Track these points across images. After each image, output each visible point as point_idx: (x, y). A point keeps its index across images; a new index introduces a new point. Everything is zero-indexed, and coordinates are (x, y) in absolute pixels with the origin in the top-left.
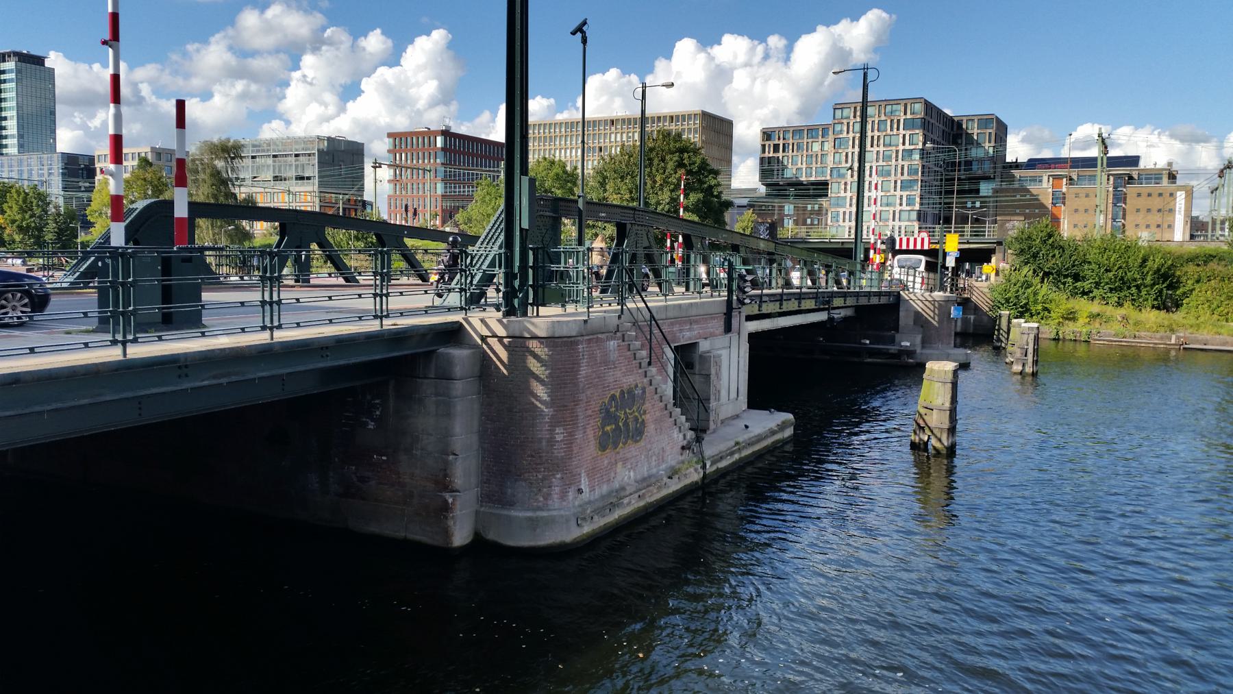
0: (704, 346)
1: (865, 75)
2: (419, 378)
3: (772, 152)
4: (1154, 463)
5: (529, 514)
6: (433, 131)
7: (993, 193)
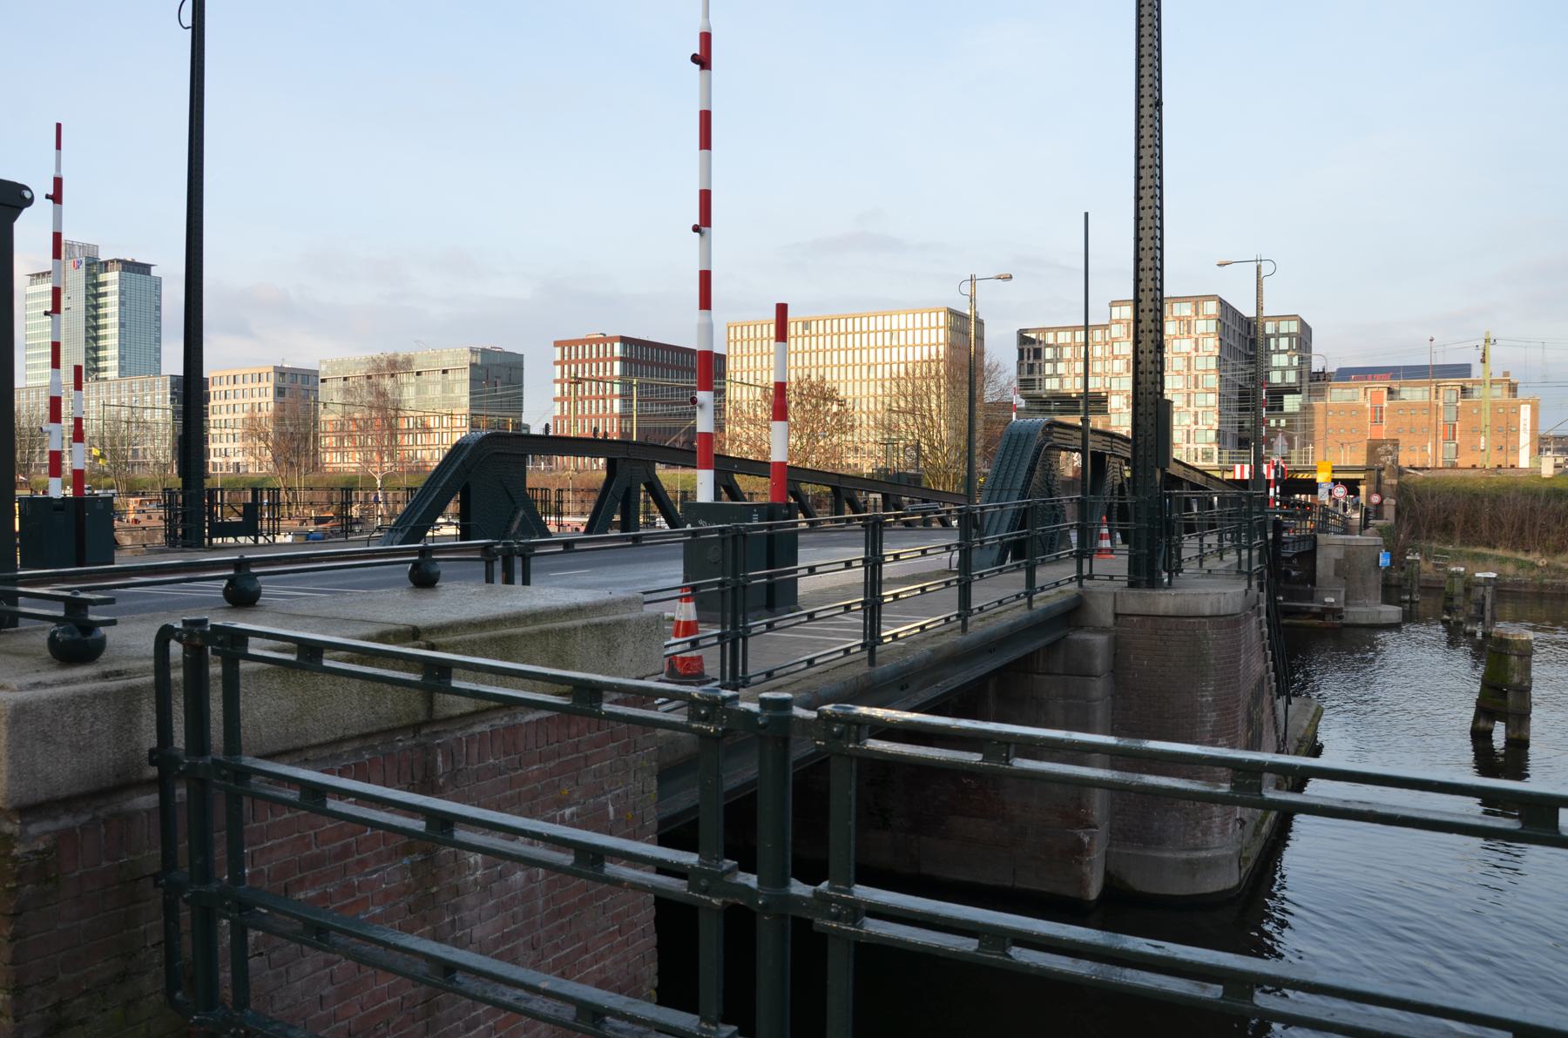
1: (1258, 268)
2: (1039, 674)
3: (1032, 358)
4: (1350, 728)
5: (1184, 855)
6: (610, 338)
7: (1301, 409)
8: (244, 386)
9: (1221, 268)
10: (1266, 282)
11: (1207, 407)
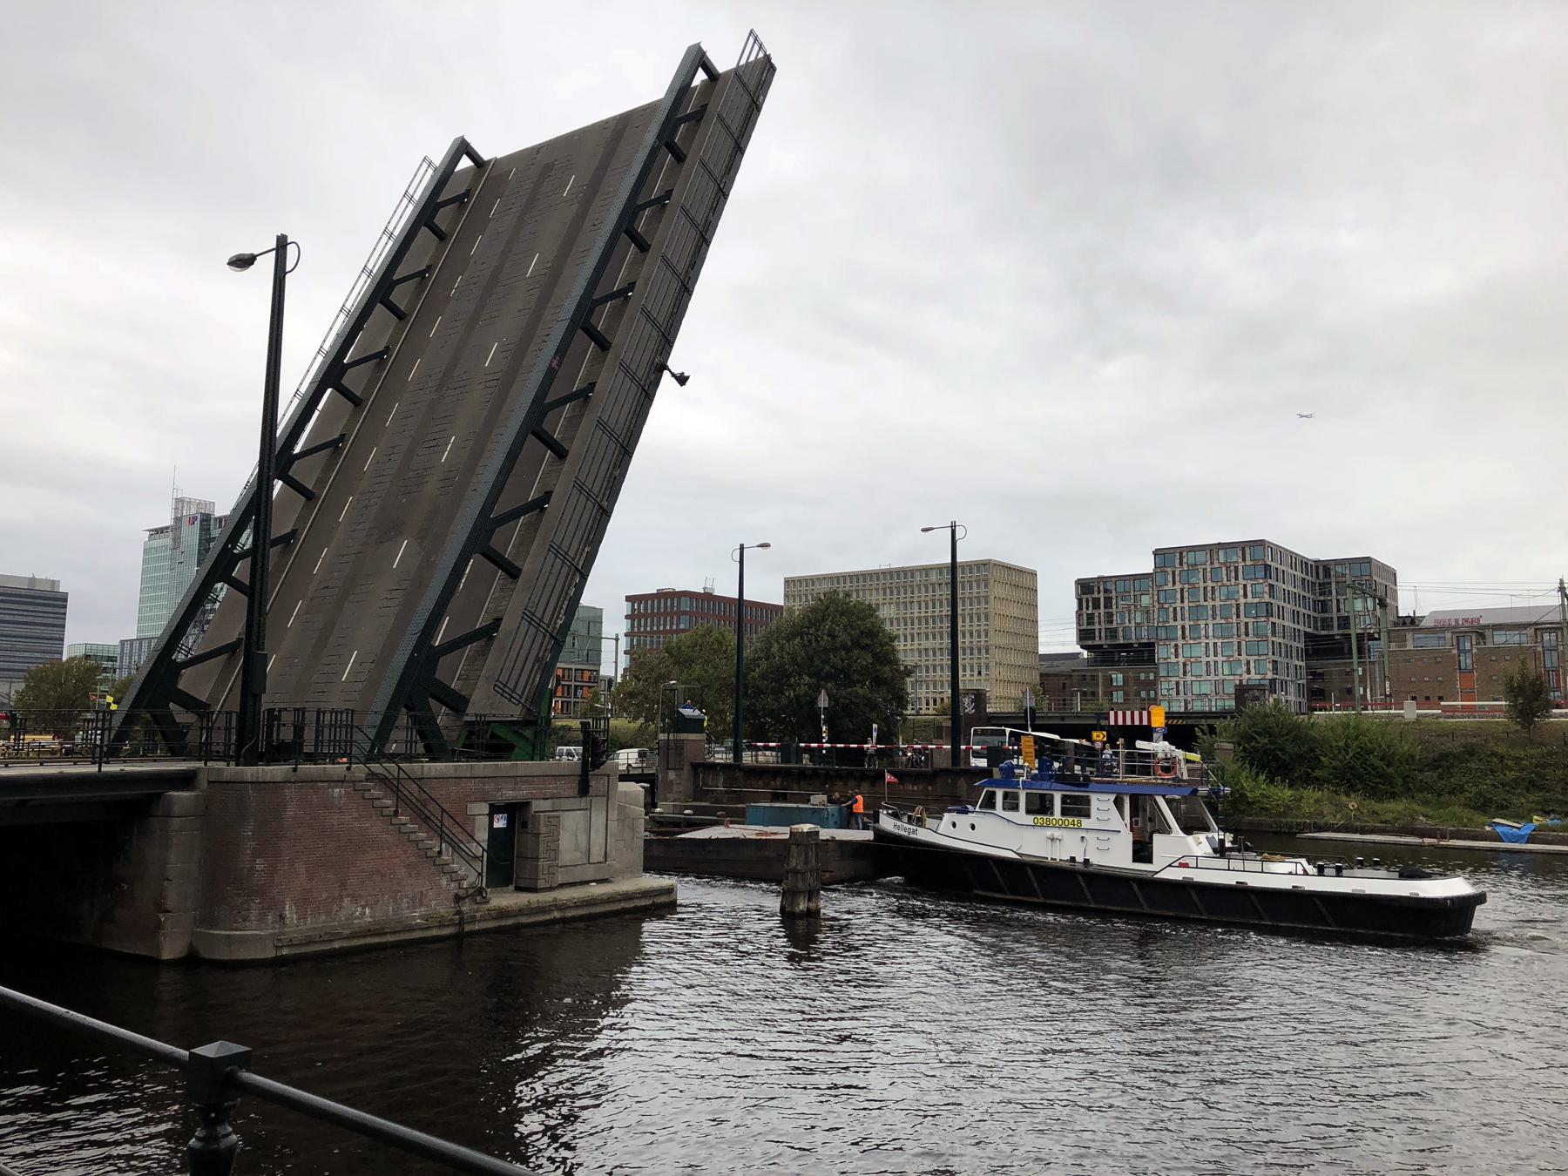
0: (537, 805)
3: (1091, 608)
8: (1216, 659)
9: (924, 533)
10: (958, 544)
11: (1259, 655)
